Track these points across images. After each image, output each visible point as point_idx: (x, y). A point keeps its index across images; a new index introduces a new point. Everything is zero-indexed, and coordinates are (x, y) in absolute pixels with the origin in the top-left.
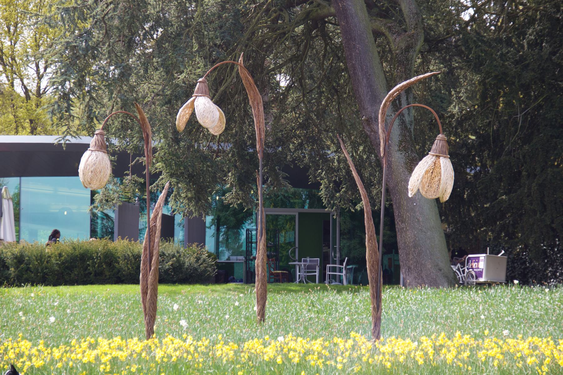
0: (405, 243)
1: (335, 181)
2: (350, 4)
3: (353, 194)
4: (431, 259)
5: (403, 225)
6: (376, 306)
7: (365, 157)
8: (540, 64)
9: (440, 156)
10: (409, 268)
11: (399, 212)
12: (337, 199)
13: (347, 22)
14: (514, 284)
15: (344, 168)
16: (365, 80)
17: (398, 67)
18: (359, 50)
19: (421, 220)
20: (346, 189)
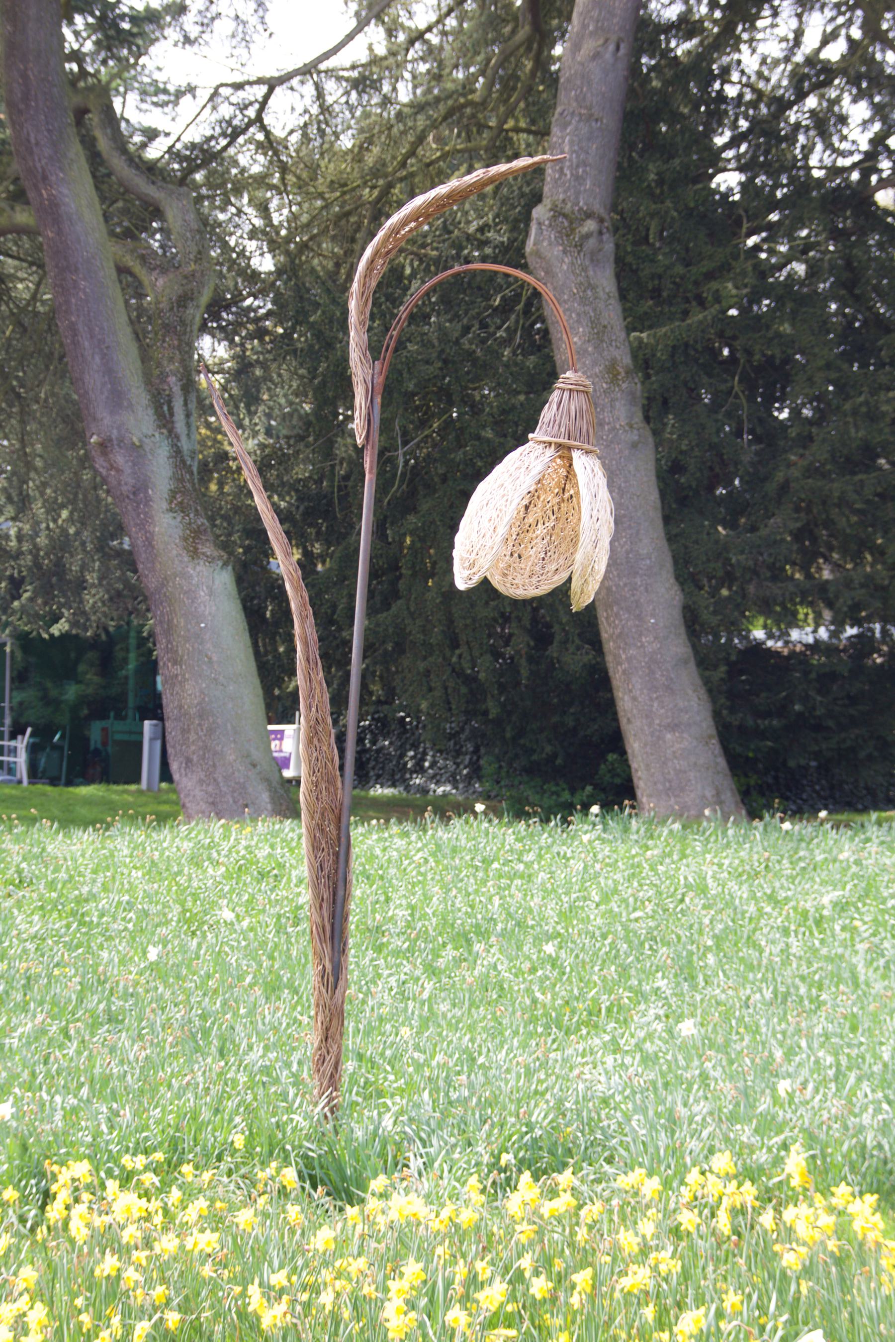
0: (181, 707)
1: (11, 577)
2: (66, 191)
3: (45, 603)
4: (235, 742)
5: (177, 670)
6: (328, 966)
7: (72, 531)
8: (443, 351)
9: (569, 448)
10: (188, 761)
11: (169, 642)
12: (14, 612)
13: (60, 232)
14: (475, 814)
15: (30, 552)
16: (97, 359)
17: (164, 336)
18: (85, 293)
19: (215, 659)
20: (34, 592)
